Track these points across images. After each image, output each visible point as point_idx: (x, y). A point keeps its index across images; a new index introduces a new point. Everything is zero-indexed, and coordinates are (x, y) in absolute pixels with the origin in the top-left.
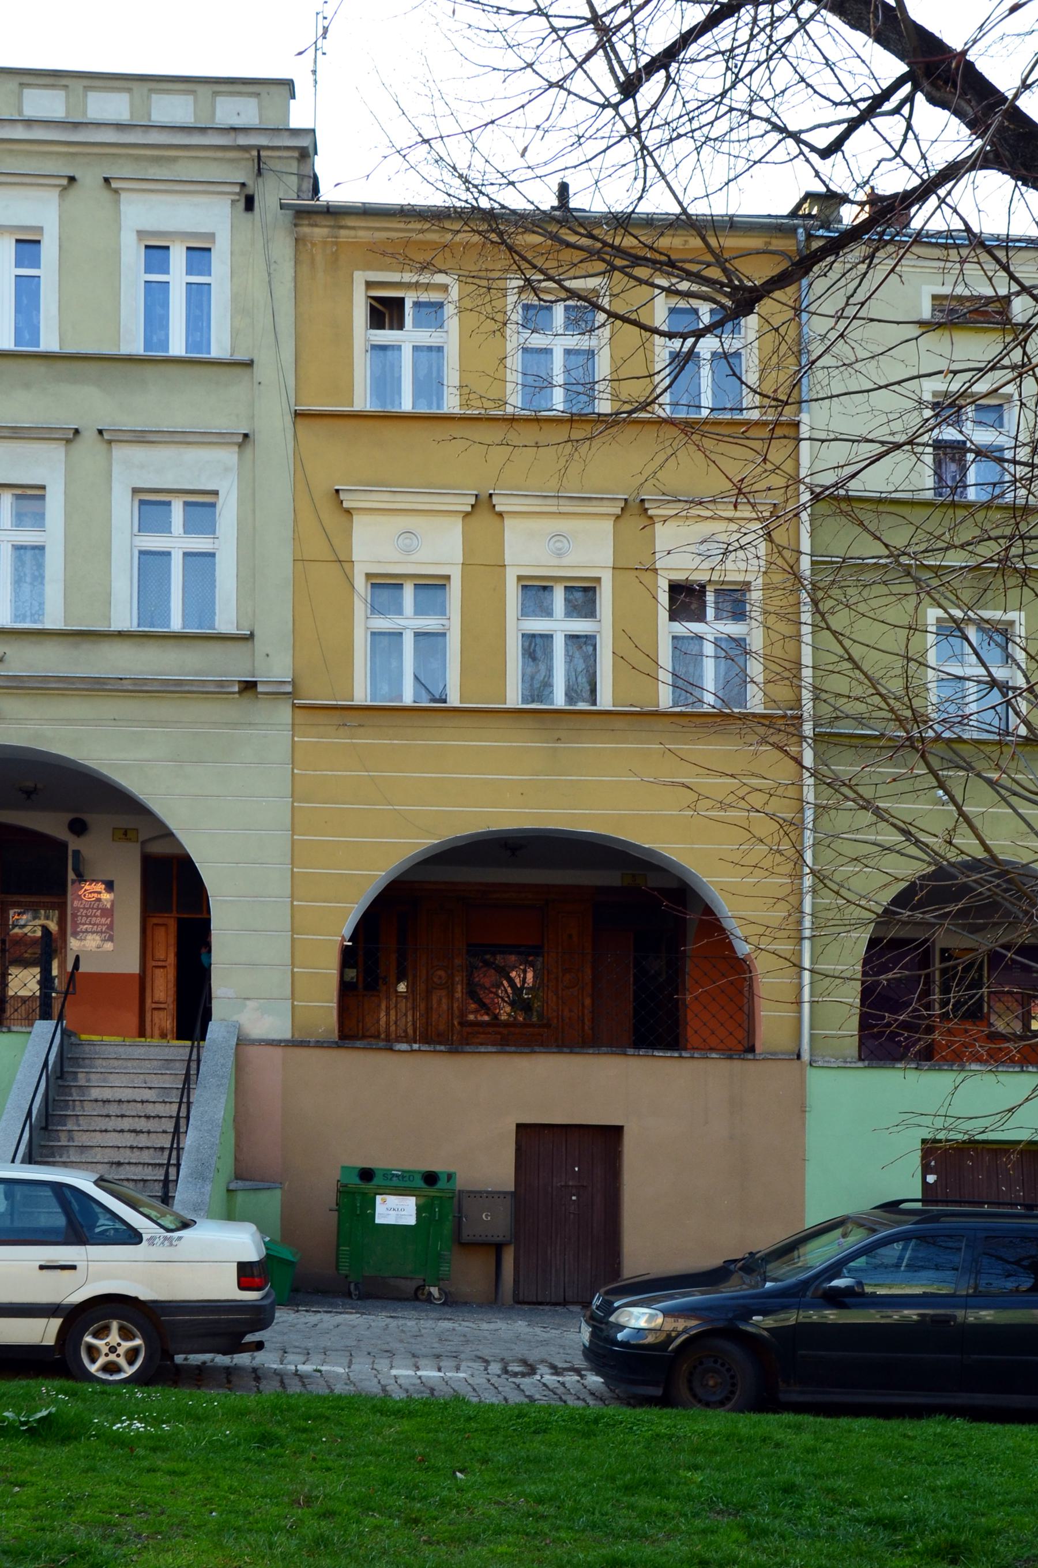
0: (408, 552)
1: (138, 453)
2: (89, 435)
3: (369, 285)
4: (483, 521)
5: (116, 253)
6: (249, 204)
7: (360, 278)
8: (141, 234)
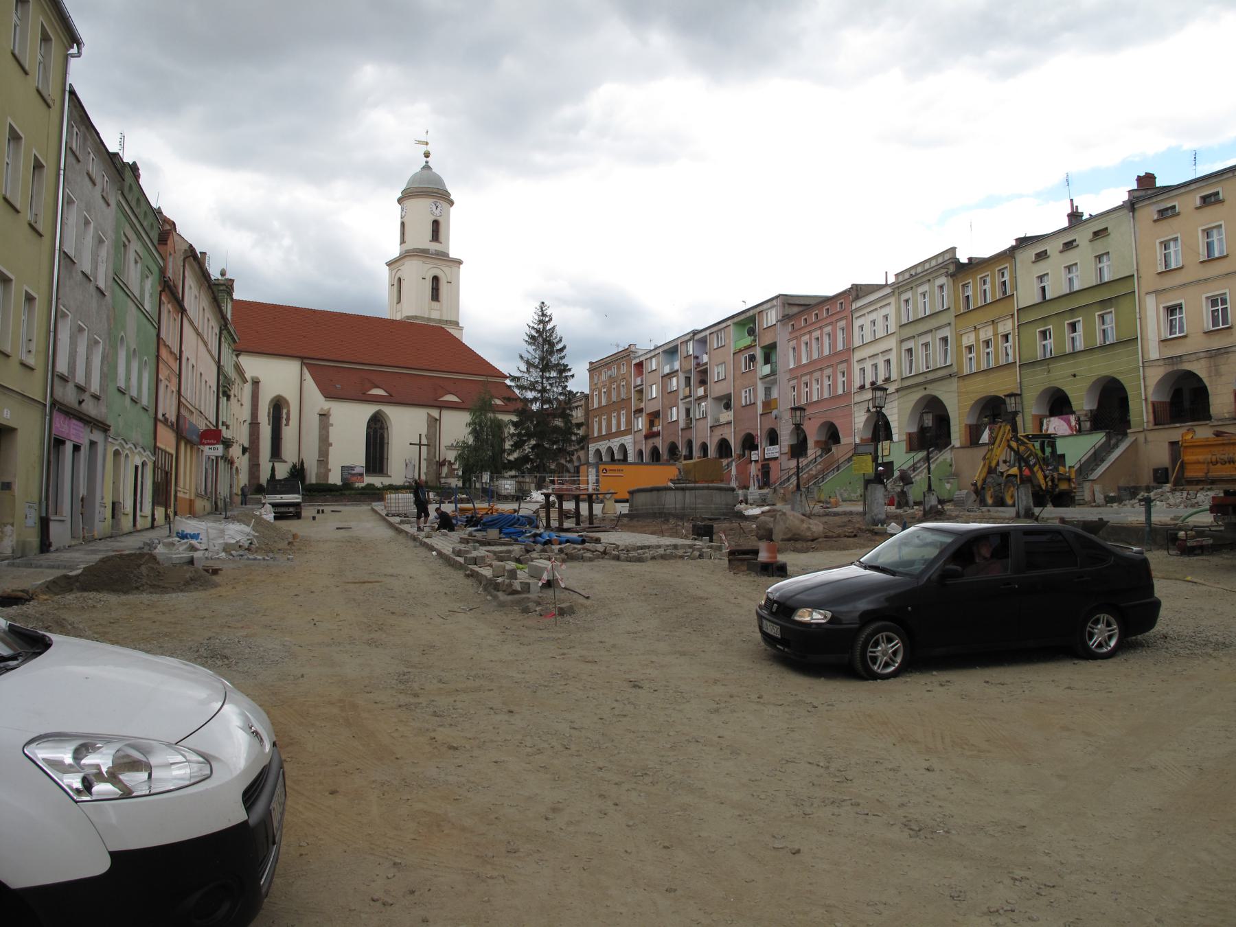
2: (916, 336)
7: (960, 285)
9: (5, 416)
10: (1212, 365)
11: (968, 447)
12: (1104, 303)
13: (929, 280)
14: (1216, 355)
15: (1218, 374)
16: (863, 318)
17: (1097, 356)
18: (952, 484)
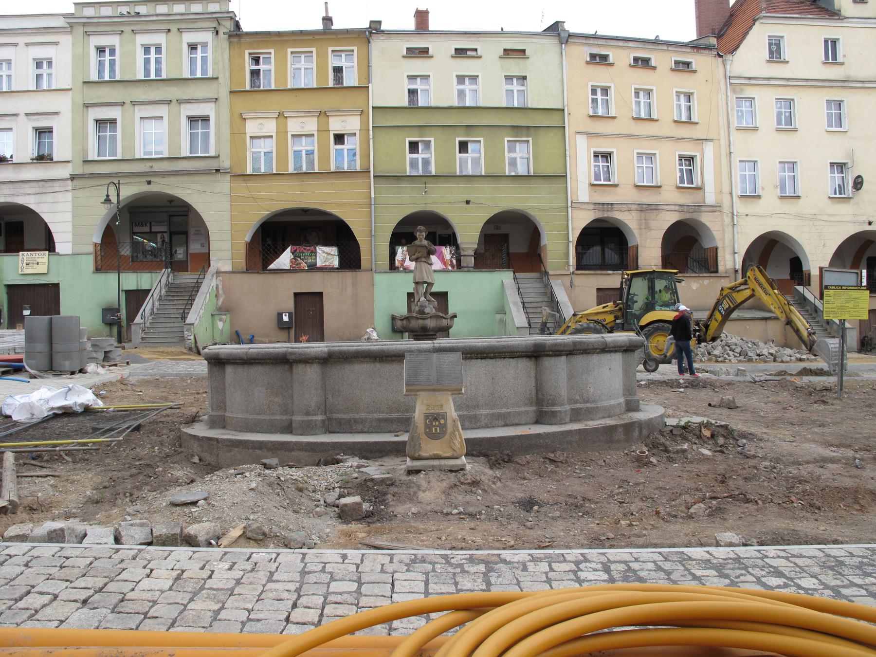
0: (261, 129)
1: (188, 106)
2: (174, 101)
3: (250, 54)
4: (281, 119)
5: (181, 49)
6: (217, 32)
7: (247, 52)
8: (142, 45)
10: (643, 218)
11: (244, 272)
12: (516, 129)
13: (169, 30)
14: (646, 210)
15: (648, 228)
16: (13, 49)
17: (503, 185)
18: (224, 322)
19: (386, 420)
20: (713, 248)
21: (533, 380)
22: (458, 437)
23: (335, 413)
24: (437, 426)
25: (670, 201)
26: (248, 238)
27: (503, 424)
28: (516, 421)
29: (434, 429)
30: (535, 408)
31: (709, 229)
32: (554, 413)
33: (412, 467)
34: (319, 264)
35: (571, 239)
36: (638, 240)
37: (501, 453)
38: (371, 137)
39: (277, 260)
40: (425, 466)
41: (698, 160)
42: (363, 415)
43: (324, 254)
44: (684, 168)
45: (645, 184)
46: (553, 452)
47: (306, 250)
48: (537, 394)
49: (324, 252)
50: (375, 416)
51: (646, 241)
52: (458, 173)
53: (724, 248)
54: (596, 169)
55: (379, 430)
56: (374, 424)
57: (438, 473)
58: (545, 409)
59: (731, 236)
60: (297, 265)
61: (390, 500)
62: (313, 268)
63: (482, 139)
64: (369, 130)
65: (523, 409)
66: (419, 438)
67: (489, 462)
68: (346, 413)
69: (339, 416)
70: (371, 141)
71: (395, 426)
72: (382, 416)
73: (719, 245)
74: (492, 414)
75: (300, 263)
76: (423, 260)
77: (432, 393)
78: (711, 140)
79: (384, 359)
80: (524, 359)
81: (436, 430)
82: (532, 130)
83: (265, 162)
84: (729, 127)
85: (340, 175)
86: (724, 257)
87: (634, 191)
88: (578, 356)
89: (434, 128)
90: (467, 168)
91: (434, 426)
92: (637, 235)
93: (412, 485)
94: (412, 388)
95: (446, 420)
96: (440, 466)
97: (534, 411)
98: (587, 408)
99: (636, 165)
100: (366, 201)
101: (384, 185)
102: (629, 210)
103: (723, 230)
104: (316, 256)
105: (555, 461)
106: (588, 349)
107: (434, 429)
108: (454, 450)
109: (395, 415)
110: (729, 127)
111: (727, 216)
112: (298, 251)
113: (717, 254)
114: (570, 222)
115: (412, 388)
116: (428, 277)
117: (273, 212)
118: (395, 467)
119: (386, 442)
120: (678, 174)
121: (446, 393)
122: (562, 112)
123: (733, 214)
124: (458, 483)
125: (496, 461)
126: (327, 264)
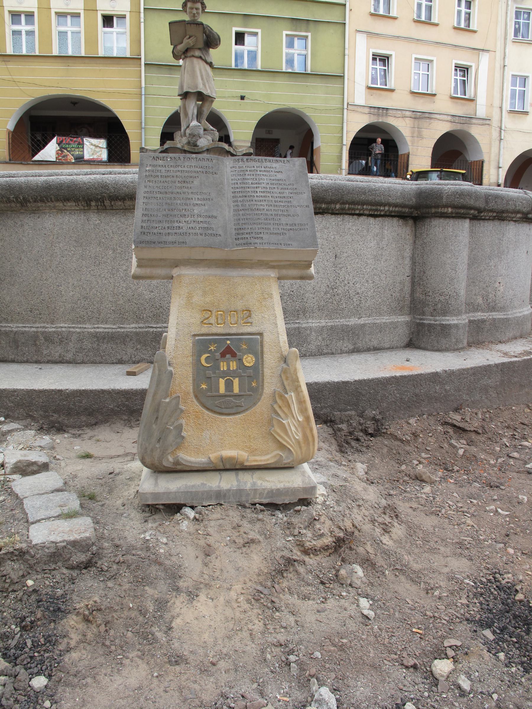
9: (222, 369)
10: (416, 126)
15: (420, 136)
17: (280, 82)
19: (111, 338)
20: (479, 161)
21: (407, 261)
22: (295, 407)
23: (6, 320)
24: (234, 374)
25: (443, 111)
26: (11, 125)
27: (351, 347)
28: (375, 343)
29: (222, 382)
30: (407, 318)
31: (394, 127)
32: (445, 329)
33: (156, 495)
34: (87, 157)
35: (345, 143)
36: (410, 147)
37: (361, 415)
38: (142, 20)
39: (42, 152)
40: (195, 494)
41: (472, 72)
42: (63, 326)
43: (92, 147)
44: (459, 78)
45: (420, 91)
46: (457, 410)
47: (71, 142)
48: (413, 291)
49: (92, 144)
50: (89, 328)
51: (417, 149)
52: (233, 67)
53: (489, 162)
54: (374, 72)
55: (98, 359)
56: (87, 344)
57: (234, 515)
58: (428, 320)
59: (497, 151)
60: (64, 157)
61: (75, 637)
62: (80, 160)
63: (259, 31)
64: (140, 12)
65: (386, 319)
66: (177, 411)
67: (335, 435)
68: (28, 321)
69: (14, 327)
70: (142, 25)
71: (130, 351)
72: (103, 328)
73: (486, 158)
74: (332, 327)
75: (67, 156)
76: (197, 53)
77: (218, 272)
78: (488, 51)
79: (107, 203)
80: (395, 220)
81: (229, 385)
82: (312, 25)
83: (27, 42)
84: (505, 39)
85: (109, 61)
86: (489, 170)
87: (409, 97)
88: (486, 224)
89: (210, 15)
90: (243, 63)
91: (224, 374)
92: (409, 143)
93: (154, 570)
94: (156, 253)
95: (259, 355)
96: (240, 492)
97: (407, 323)
98: (494, 320)
99: (413, 71)
100: (136, 90)
101: (155, 74)
102: (404, 117)
103: (490, 144)
104: (83, 148)
105: (464, 430)
106: (507, 211)
107: (222, 382)
108: (282, 447)
109: (131, 327)
110: (505, 39)
111: (495, 130)
112: (64, 142)
113: (482, 167)
114: (345, 124)
115: (156, 253)
116: (204, 85)
117: (37, 99)
118: (116, 465)
119: (103, 391)
120: (453, 84)
121: (258, 273)
122: (342, 7)
123: (501, 129)
124: (297, 554)
125: (351, 433)
126: (95, 157)
